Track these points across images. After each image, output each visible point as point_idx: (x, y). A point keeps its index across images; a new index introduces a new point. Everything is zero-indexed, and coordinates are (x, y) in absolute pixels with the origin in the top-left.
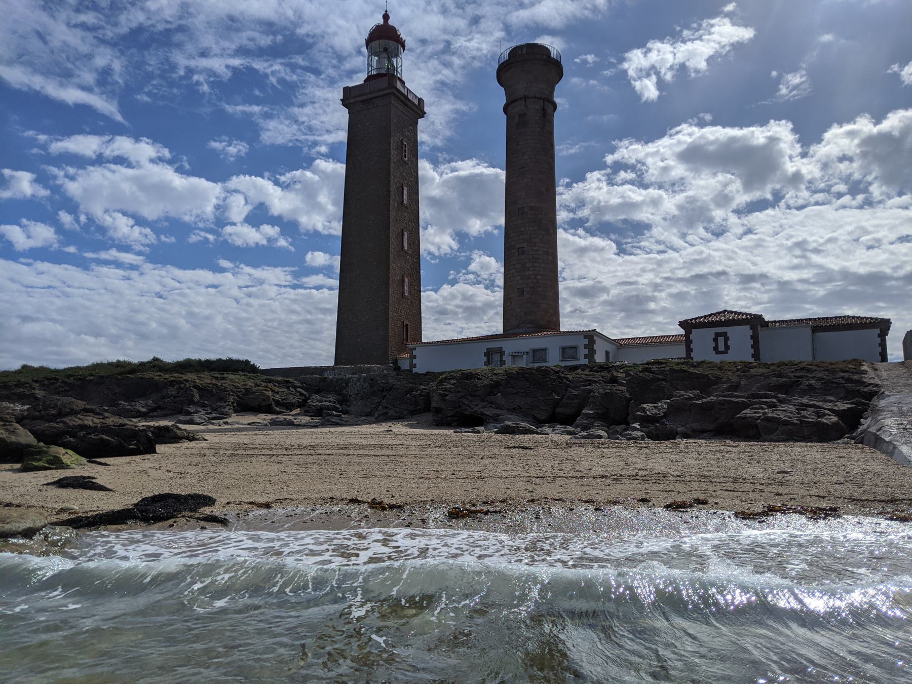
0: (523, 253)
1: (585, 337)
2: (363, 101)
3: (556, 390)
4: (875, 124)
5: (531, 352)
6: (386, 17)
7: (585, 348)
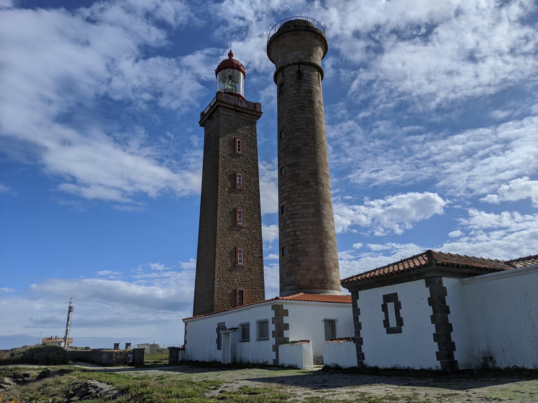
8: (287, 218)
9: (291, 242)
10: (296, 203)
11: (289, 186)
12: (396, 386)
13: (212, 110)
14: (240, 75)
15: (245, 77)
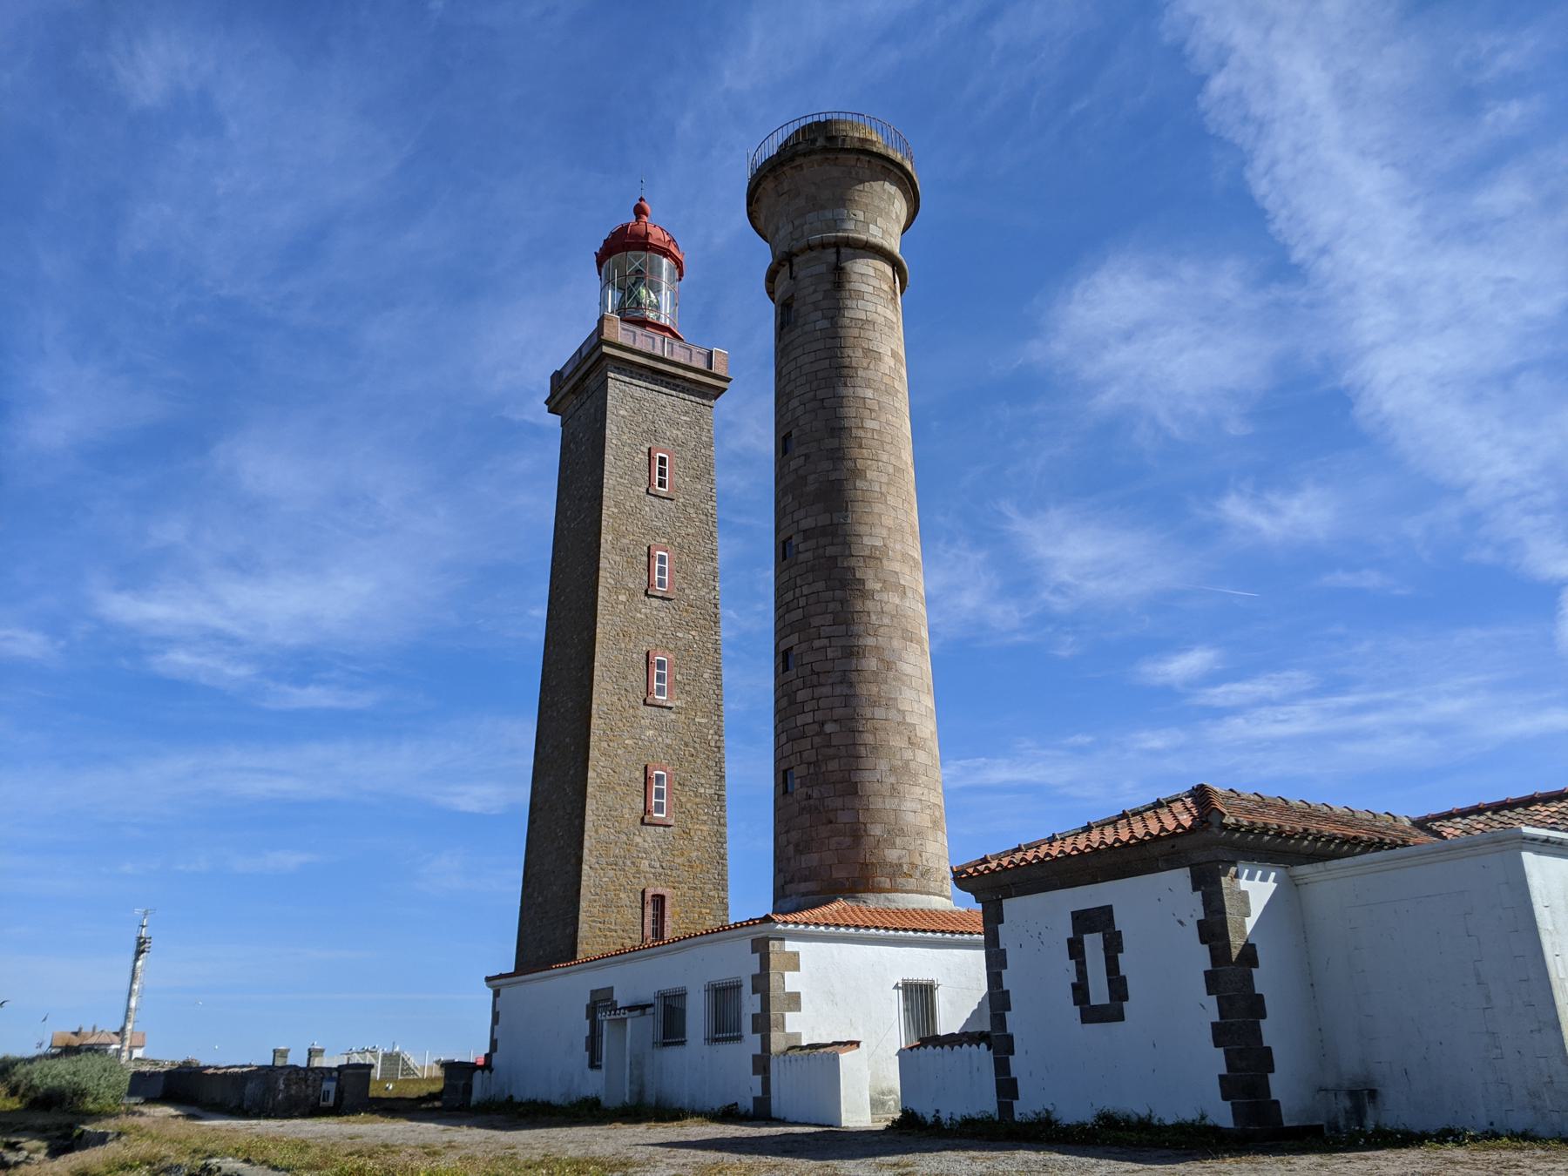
10: (825, 642)
11: (806, 591)
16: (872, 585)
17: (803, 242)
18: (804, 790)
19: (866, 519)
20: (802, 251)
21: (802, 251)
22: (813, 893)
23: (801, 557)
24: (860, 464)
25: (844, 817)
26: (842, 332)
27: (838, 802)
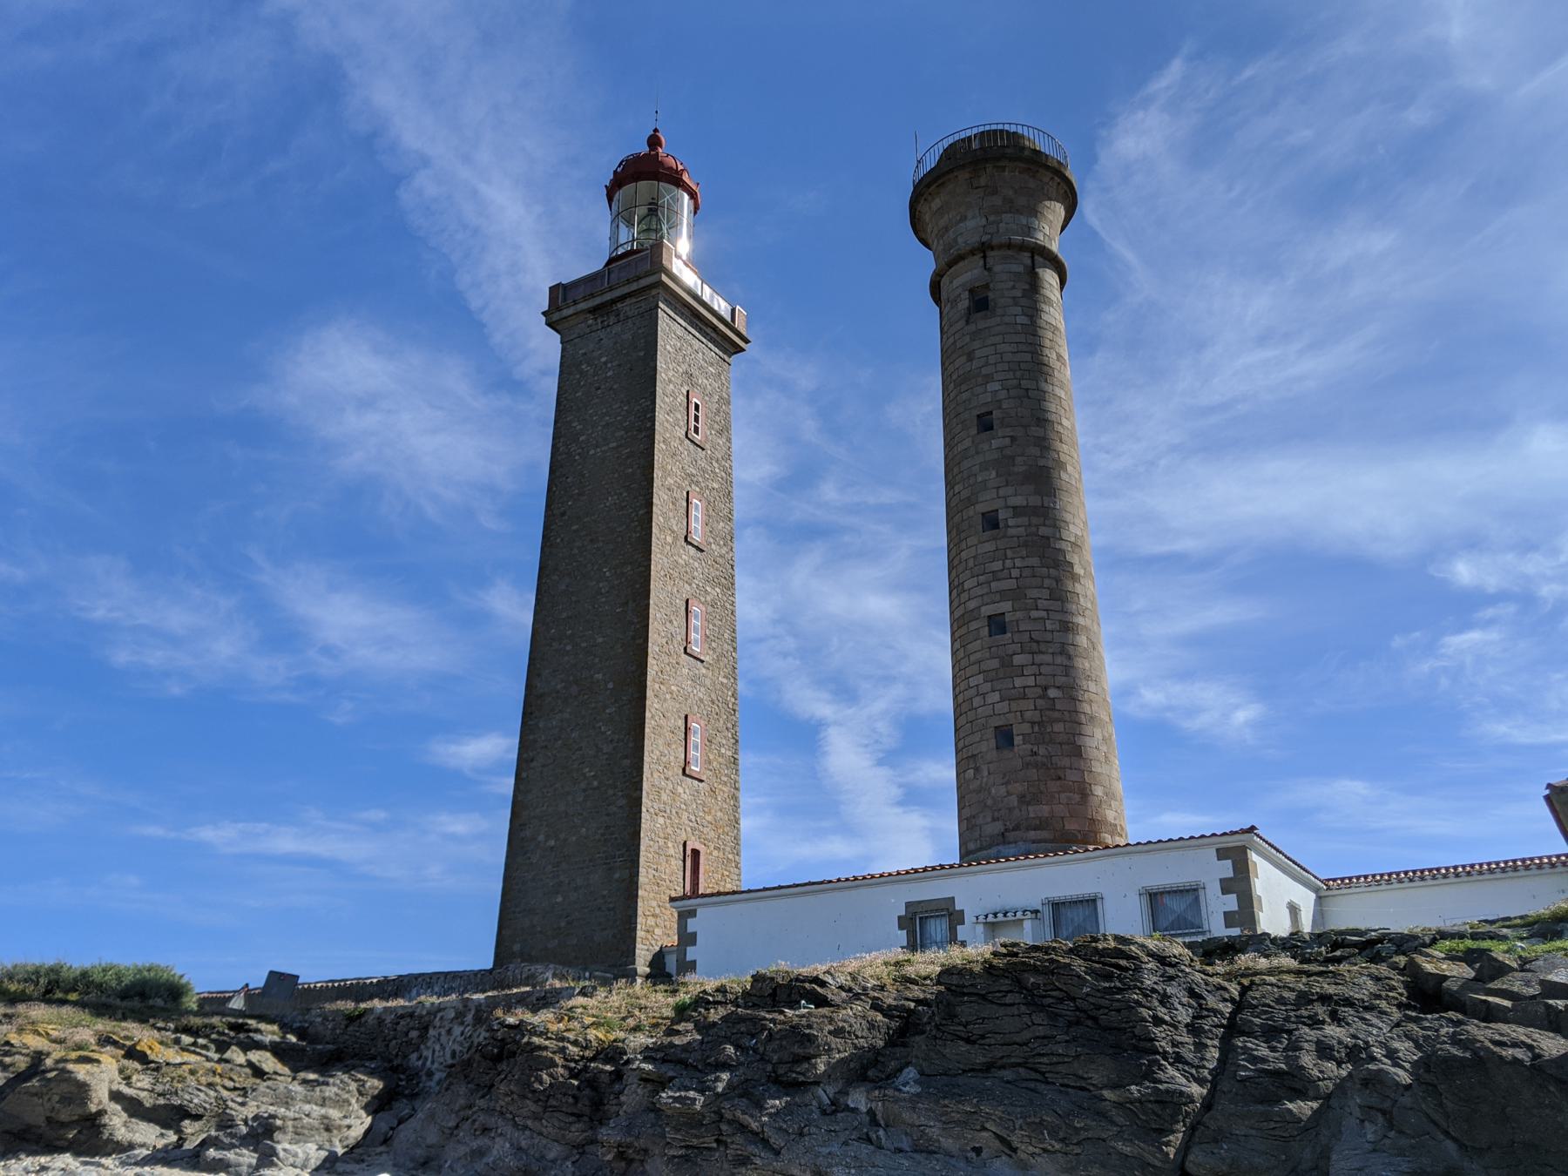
0: (1002, 629)
1: (1222, 854)
2: (593, 310)
3: (699, 896)
4: (1227, 927)
5: (1047, 913)
6: (654, 141)
7: (1225, 891)
8: (1017, 647)
9: (1036, 716)
10: (1044, 614)
11: (1018, 563)
12: (378, 815)
13: (722, 327)
14: (677, 200)
15: (696, 208)
16: (1078, 570)
17: (1004, 239)
18: (1029, 747)
19: (1069, 508)
20: (1001, 247)
21: (1001, 247)
22: (1045, 841)
23: (1011, 531)
24: (1063, 458)
25: (1072, 776)
26: (1041, 332)
27: (1066, 762)
